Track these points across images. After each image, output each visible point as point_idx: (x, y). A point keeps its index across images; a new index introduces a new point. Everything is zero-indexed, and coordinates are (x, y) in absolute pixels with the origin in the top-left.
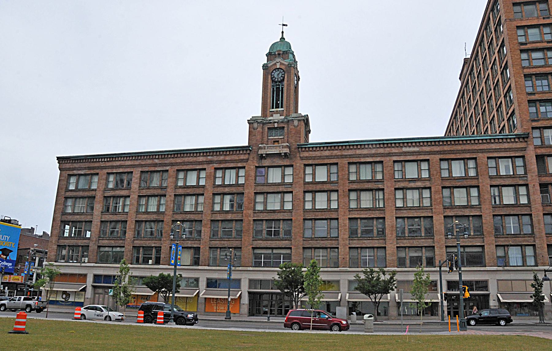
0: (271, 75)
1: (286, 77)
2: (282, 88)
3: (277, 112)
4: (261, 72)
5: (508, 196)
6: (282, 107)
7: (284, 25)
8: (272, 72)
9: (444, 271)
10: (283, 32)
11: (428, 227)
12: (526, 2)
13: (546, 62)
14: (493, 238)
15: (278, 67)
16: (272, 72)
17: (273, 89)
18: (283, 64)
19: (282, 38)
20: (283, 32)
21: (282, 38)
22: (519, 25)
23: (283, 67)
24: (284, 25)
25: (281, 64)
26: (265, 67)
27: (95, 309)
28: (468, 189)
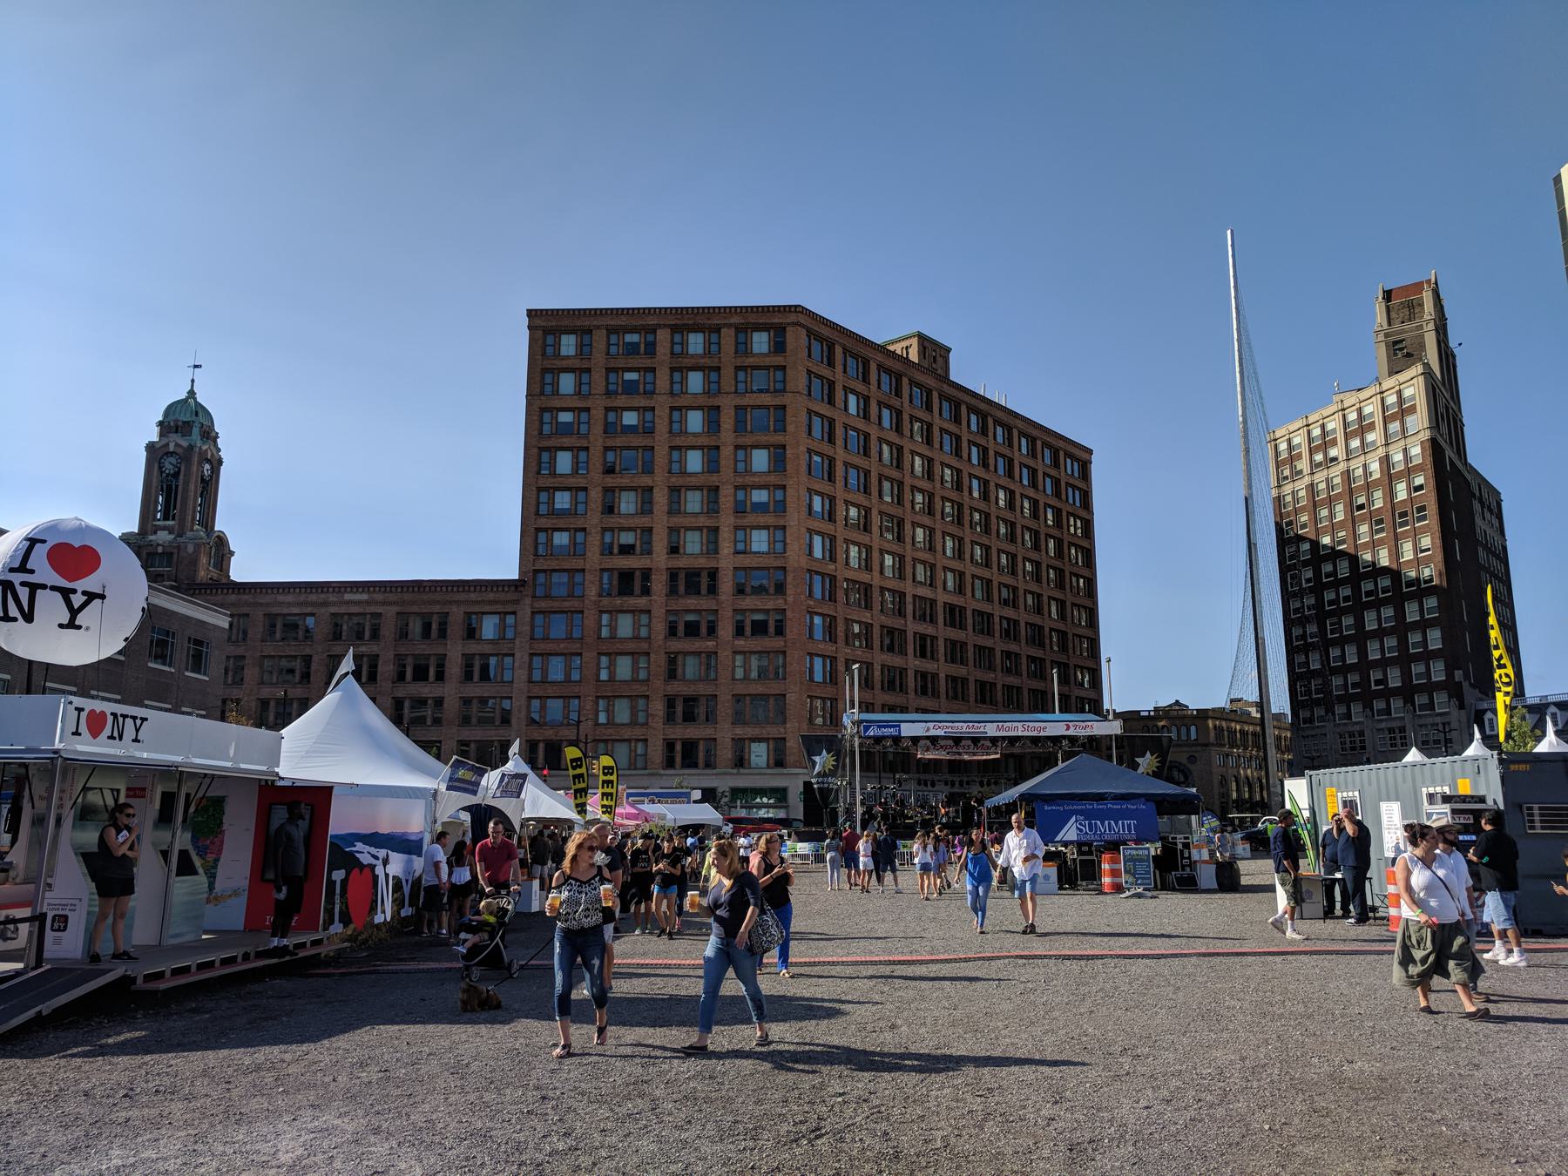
0: (160, 463)
1: (183, 468)
2: (177, 486)
3: (164, 528)
4: (142, 457)
5: (624, 668)
6: (173, 519)
7: (196, 366)
8: (161, 458)
9: (622, 775)
10: (193, 381)
11: (305, 670)
12: (1445, 326)
13: (1377, 483)
14: (391, 685)
15: (171, 450)
16: (161, 458)
17: (162, 487)
18: (180, 446)
19: (192, 393)
20: (193, 381)
21: (192, 393)
22: (610, 405)
23: (179, 451)
24: (196, 366)
25: (177, 445)
26: (150, 447)
27: (329, 907)
28: (568, 657)
